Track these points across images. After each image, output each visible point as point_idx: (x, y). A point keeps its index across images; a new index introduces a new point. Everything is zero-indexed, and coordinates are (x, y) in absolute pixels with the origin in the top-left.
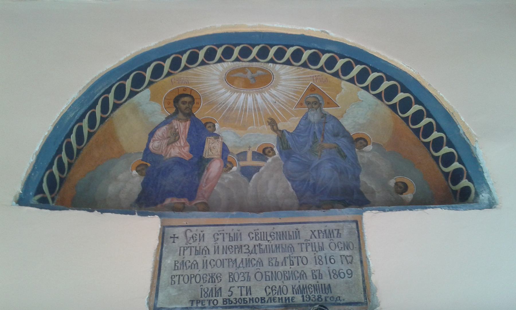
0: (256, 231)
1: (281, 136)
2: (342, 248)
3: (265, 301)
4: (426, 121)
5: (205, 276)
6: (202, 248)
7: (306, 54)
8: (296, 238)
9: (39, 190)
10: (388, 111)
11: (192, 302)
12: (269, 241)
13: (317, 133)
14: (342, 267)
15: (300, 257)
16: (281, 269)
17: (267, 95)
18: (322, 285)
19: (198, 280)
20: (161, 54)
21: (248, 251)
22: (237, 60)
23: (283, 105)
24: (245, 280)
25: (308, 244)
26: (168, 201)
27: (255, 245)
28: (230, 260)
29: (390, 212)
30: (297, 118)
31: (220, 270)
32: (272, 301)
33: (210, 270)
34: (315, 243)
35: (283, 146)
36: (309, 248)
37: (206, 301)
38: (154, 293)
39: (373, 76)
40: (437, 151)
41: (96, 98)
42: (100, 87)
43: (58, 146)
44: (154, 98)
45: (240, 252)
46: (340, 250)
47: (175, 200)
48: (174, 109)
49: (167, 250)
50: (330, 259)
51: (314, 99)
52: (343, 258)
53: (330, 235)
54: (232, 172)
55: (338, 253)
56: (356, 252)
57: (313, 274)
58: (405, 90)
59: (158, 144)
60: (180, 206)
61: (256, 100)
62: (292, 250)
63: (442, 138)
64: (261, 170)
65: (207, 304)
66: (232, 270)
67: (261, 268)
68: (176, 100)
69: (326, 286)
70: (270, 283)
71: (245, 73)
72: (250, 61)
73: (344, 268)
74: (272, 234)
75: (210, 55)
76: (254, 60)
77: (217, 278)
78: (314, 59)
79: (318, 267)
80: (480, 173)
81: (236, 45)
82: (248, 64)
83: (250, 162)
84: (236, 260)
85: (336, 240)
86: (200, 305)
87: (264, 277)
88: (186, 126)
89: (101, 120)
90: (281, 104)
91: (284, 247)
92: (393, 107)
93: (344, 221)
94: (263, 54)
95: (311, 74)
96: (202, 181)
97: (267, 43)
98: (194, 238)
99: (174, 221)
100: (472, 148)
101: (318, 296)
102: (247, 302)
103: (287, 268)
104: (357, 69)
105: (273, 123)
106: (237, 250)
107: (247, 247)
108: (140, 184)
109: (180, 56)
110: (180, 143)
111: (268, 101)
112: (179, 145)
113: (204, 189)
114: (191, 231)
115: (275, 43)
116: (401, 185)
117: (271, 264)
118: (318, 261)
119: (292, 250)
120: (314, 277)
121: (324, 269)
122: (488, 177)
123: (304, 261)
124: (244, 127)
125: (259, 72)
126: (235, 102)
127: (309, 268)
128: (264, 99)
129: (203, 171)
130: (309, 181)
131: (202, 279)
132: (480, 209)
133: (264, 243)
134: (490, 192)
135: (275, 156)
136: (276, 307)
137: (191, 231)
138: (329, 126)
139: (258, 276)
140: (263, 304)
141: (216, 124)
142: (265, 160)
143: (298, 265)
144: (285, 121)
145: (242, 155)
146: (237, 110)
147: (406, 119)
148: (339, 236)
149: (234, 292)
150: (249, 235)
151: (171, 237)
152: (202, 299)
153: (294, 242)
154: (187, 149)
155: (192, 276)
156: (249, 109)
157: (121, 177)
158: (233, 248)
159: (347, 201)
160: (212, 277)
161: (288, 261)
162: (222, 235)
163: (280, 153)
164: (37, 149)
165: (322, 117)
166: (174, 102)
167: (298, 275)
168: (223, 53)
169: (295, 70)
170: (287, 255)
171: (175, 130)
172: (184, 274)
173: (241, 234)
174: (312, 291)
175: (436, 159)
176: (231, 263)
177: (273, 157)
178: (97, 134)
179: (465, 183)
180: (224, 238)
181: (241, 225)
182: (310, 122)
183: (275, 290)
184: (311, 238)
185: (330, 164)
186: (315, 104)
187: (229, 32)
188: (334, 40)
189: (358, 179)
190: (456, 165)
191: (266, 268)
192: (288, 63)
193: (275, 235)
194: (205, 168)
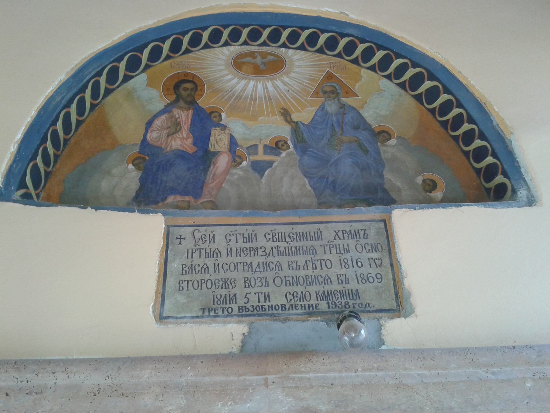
0: (273, 232)
1: (296, 127)
2: (369, 250)
3: (285, 309)
4: (456, 111)
5: (217, 281)
6: (212, 250)
7: (323, 38)
8: (318, 239)
9: (22, 185)
10: (413, 102)
11: (203, 310)
12: (287, 242)
13: (335, 125)
14: (371, 271)
15: (324, 260)
16: (302, 273)
17: (279, 83)
18: (348, 290)
19: (209, 285)
20: (159, 34)
21: (264, 254)
22: (245, 43)
23: (297, 93)
24: (262, 286)
25: (331, 246)
26: (170, 199)
27: (272, 248)
28: (245, 264)
29: (421, 210)
30: (313, 108)
31: (234, 275)
32: (294, 309)
33: (222, 275)
34: (339, 245)
35: (298, 139)
36: (334, 251)
37: (219, 309)
38: (159, 300)
39: (397, 62)
40: (467, 145)
41: (85, 81)
42: (90, 70)
43: (43, 134)
44: (150, 83)
45: (256, 255)
46: (367, 252)
47: (179, 198)
48: (175, 96)
49: (172, 253)
50: (357, 263)
51: (331, 88)
52: (372, 261)
53: (356, 235)
54: (242, 167)
55: (365, 256)
56: (385, 254)
57: (338, 278)
58: (432, 77)
59: (157, 135)
60: (186, 205)
61: (267, 88)
62: (314, 253)
63: (473, 130)
64: (274, 165)
65: (220, 313)
66: (248, 275)
67: (280, 272)
68: (177, 87)
69: (354, 292)
70: (291, 289)
71: (255, 58)
72: (259, 45)
73: (373, 271)
74: (291, 235)
75: (215, 37)
76: (264, 44)
77: (231, 283)
78: (331, 44)
79: (343, 271)
80: (517, 168)
81: (245, 26)
82: (257, 48)
83: (261, 156)
84: (251, 263)
85: (363, 241)
86: (212, 313)
87: (284, 282)
88: (188, 115)
89: (91, 107)
90: (294, 92)
91: (305, 248)
92: (418, 98)
93: (370, 221)
94: (274, 37)
95: (328, 61)
96: (208, 177)
97: (278, 24)
98: (203, 239)
99: (180, 221)
100: (507, 141)
101: (345, 303)
102: (265, 309)
103: (310, 272)
104: (379, 54)
105: (286, 114)
106: (252, 253)
107: (263, 249)
108: (137, 180)
109: (181, 37)
110: (182, 134)
111: (280, 90)
112: (181, 136)
113: (211, 185)
114: (199, 231)
115: (287, 24)
116: (428, 182)
117: (291, 268)
118: (343, 264)
119: (314, 253)
120: (340, 282)
121: (350, 273)
122: (525, 172)
123: (326, 264)
124: (254, 118)
125: (270, 58)
126: (243, 90)
127: (336, 271)
128: (276, 87)
129: (209, 167)
130: (328, 178)
131: (214, 285)
132: (520, 207)
133: (283, 245)
134: (528, 189)
135: (289, 150)
136: (299, 314)
137: (199, 231)
138: (348, 117)
139: (278, 281)
140: (283, 312)
141: (222, 114)
142: (279, 154)
143: (322, 269)
144: (300, 112)
145: (253, 149)
146: (246, 98)
147: (432, 111)
148: (365, 237)
149: (251, 299)
150: (265, 237)
151: (177, 238)
152: (214, 306)
153: (316, 243)
154: (190, 141)
155: (203, 281)
156: (259, 97)
157: (115, 171)
158: (248, 251)
159: (371, 201)
160: (225, 283)
161: (310, 264)
162: (235, 235)
163: (295, 146)
164: (19, 136)
165: (341, 108)
166: (174, 88)
167: (322, 280)
168: (230, 35)
169: (310, 55)
170: (309, 257)
171: (176, 119)
172: (193, 279)
173: (256, 234)
174: (338, 298)
175: (466, 154)
176: (246, 267)
177: (287, 151)
178: (86, 122)
179: (500, 179)
180: (237, 239)
181: (256, 225)
182: (327, 113)
183: (297, 297)
184: (335, 239)
185: (350, 160)
186: (333, 93)
187: (237, 11)
188: (354, 23)
189: (382, 176)
190: (490, 160)
191: (286, 272)
192: (302, 48)
193: (295, 236)
194: (211, 163)
